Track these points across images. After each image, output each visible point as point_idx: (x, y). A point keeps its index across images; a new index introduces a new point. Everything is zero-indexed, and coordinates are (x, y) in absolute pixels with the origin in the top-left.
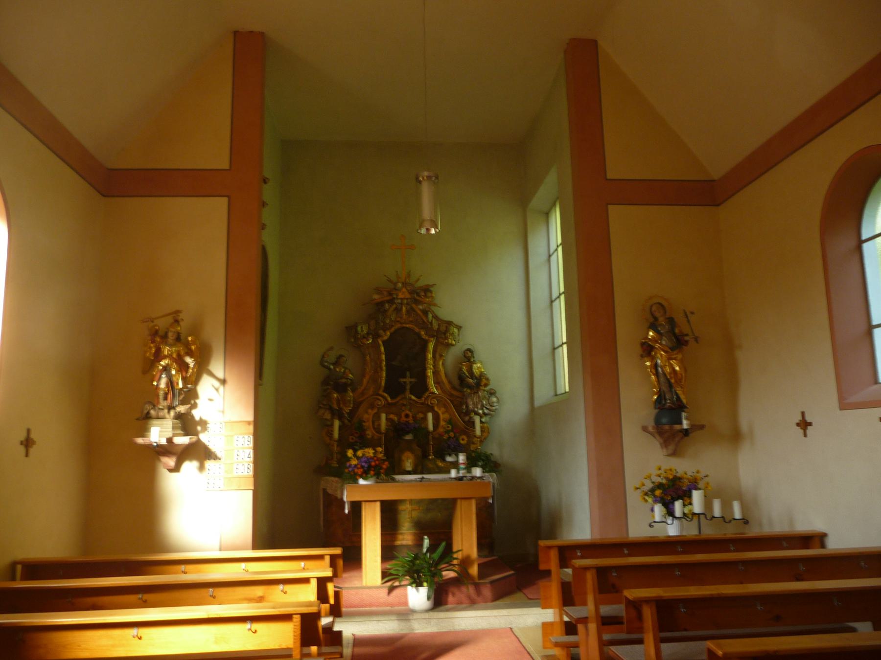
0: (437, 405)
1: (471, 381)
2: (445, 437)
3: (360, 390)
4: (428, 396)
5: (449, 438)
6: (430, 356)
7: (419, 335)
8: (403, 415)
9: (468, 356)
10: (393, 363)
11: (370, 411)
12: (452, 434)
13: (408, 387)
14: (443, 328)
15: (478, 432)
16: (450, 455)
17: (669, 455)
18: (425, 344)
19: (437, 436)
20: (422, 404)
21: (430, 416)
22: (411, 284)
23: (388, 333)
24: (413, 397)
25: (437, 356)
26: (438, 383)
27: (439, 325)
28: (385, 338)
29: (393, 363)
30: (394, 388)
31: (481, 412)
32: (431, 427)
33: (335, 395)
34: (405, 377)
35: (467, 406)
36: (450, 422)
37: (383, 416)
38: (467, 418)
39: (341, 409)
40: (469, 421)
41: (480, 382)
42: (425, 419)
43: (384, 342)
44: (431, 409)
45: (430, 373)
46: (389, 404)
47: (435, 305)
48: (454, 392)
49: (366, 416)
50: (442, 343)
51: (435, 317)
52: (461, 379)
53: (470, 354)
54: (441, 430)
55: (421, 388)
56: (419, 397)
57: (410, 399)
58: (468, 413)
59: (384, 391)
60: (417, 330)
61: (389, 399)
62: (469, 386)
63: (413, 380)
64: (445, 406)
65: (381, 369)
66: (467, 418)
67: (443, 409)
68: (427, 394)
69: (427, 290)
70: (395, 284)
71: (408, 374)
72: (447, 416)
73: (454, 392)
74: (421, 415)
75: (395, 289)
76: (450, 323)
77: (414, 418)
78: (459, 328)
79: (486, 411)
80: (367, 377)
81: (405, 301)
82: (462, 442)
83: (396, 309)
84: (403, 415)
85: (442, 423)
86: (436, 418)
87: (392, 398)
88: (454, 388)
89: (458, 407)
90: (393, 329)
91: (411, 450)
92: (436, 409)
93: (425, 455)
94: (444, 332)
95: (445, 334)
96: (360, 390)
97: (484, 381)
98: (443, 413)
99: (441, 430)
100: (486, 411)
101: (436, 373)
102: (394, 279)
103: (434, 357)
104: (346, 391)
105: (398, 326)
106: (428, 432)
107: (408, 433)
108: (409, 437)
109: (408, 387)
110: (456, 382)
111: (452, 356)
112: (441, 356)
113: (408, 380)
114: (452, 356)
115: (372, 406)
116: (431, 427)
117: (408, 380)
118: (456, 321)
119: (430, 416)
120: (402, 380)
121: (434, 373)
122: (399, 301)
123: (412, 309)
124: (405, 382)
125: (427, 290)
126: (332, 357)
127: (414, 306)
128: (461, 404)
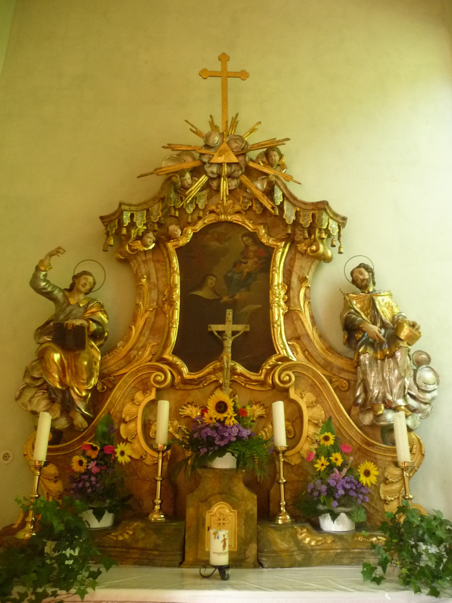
0: (296, 385)
1: (375, 328)
2: (321, 464)
3: (122, 351)
4: (274, 367)
5: (331, 467)
6: (278, 278)
7: (254, 236)
8: (211, 405)
9: (361, 280)
10: (199, 293)
11: (139, 396)
12: (338, 458)
13: (228, 343)
14: (306, 221)
15: (404, 454)
16: (334, 516)
17: (27, 367)
18: (268, 254)
19: (295, 461)
20: (262, 383)
21: (279, 408)
22: (241, 138)
23: (190, 232)
24: (240, 368)
25: (295, 280)
26: (297, 338)
27: (297, 214)
28: (183, 241)
29: (199, 293)
30: (197, 346)
31: (401, 402)
32: (281, 440)
33: (57, 357)
34: (223, 321)
35: (366, 390)
36: (328, 424)
37: (164, 407)
38: (368, 419)
39: (67, 389)
40: (372, 426)
41: (393, 337)
42: (268, 417)
43: (179, 250)
44: (282, 393)
45: (278, 313)
46: (185, 382)
47: (289, 178)
48: (331, 358)
49: (129, 408)
50: (304, 254)
51: (288, 197)
52: (351, 328)
53: (367, 275)
54: (305, 447)
55: (257, 348)
56: (255, 368)
57: (233, 371)
58: (368, 405)
59: (175, 352)
60: (250, 226)
61: (185, 370)
62: (374, 344)
63: (241, 328)
64: (313, 387)
65: (172, 304)
66: (368, 419)
67: (310, 397)
68: (272, 360)
69: (270, 151)
70: (207, 138)
71: (229, 313)
72: (319, 413)
73: (331, 358)
74: (258, 411)
75: (207, 146)
76: (322, 206)
77: (240, 414)
78: (342, 222)
79: (412, 403)
80: (141, 323)
81: (226, 170)
82: (363, 479)
83: (207, 186)
84: (211, 405)
85: (308, 429)
86: (295, 418)
87: (191, 370)
88: (330, 349)
89: (345, 391)
90: (199, 226)
91: (227, 495)
92: (293, 394)
93: (266, 513)
94: (309, 229)
95: (311, 229)
96: (122, 351)
97: (405, 332)
98: (310, 406)
99: (305, 447)
100: (412, 403)
101: (291, 315)
102: (206, 129)
103: (287, 281)
104: (81, 345)
105: (209, 219)
106: (276, 451)
107: (221, 452)
108: (225, 462)
109: (228, 343)
110: (338, 337)
111: (326, 283)
112: (303, 280)
113: (229, 328)
114: (326, 283)
115: (144, 386)
116: (281, 440)
117: (229, 328)
118: (336, 207)
119: (279, 408)
120: (215, 328)
121: (286, 315)
122: (215, 169)
123: (242, 186)
124: (221, 333)
125: (270, 151)
126: (59, 276)
127: (245, 179)
128: (352, 387)
